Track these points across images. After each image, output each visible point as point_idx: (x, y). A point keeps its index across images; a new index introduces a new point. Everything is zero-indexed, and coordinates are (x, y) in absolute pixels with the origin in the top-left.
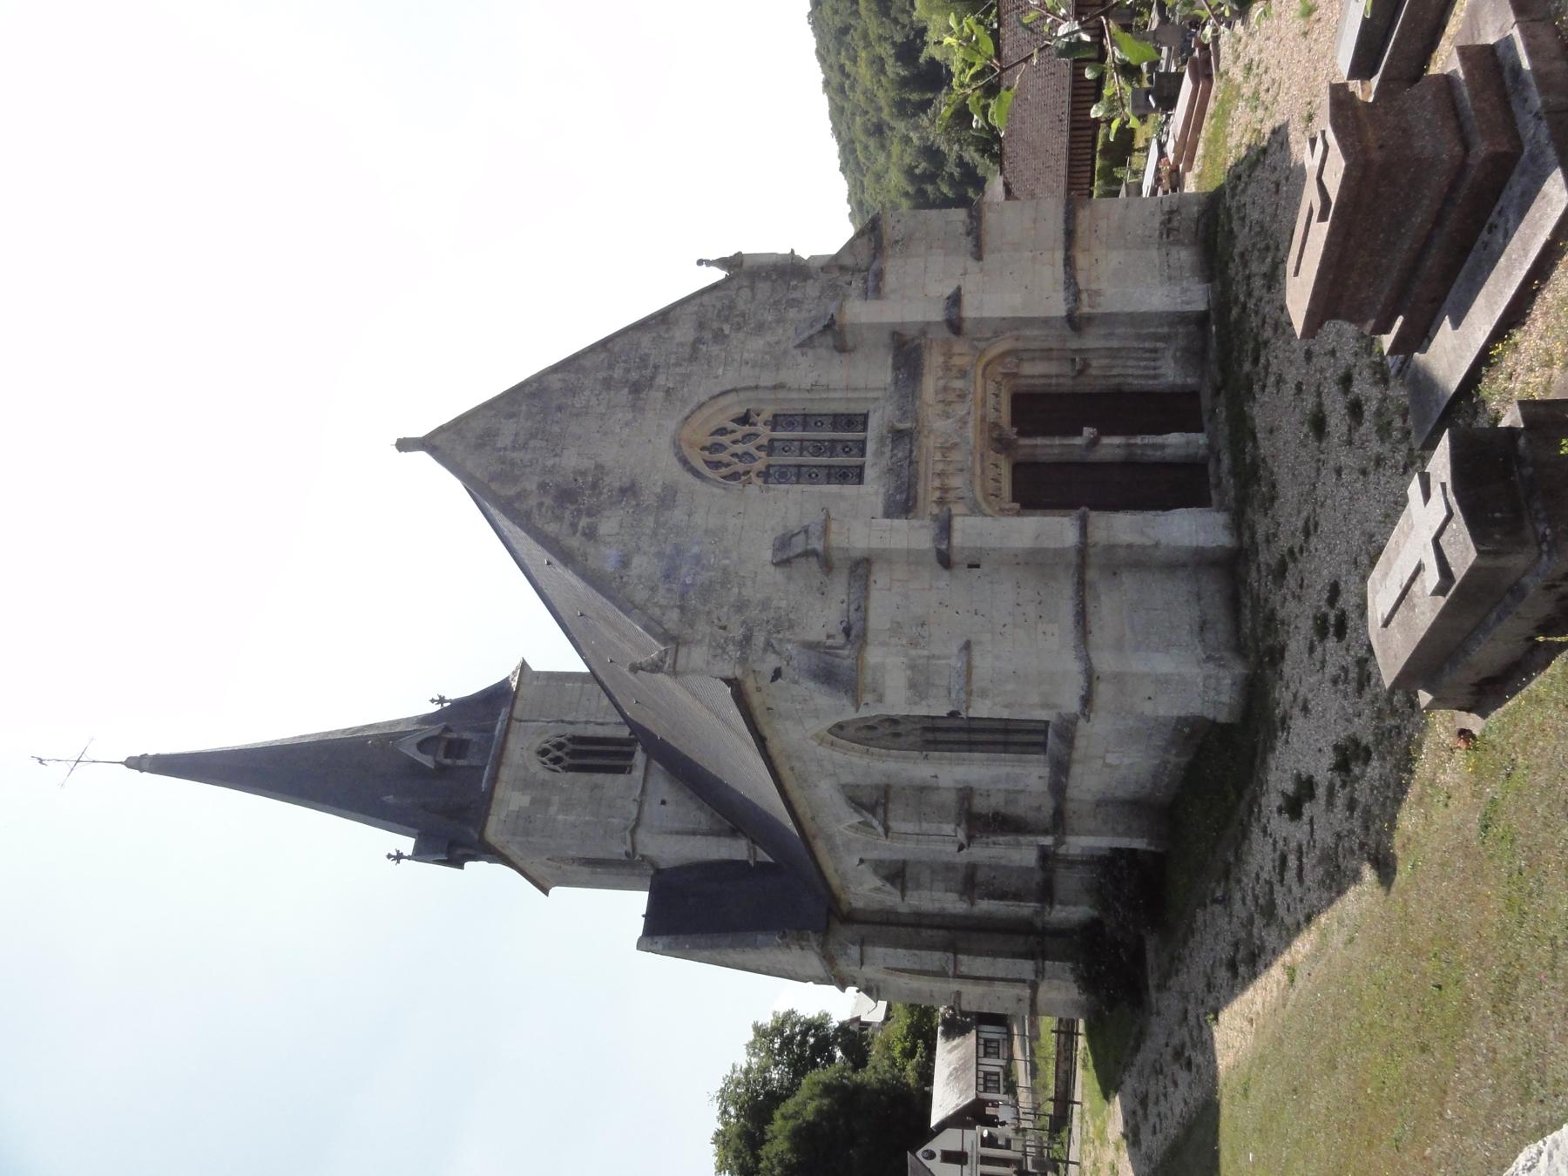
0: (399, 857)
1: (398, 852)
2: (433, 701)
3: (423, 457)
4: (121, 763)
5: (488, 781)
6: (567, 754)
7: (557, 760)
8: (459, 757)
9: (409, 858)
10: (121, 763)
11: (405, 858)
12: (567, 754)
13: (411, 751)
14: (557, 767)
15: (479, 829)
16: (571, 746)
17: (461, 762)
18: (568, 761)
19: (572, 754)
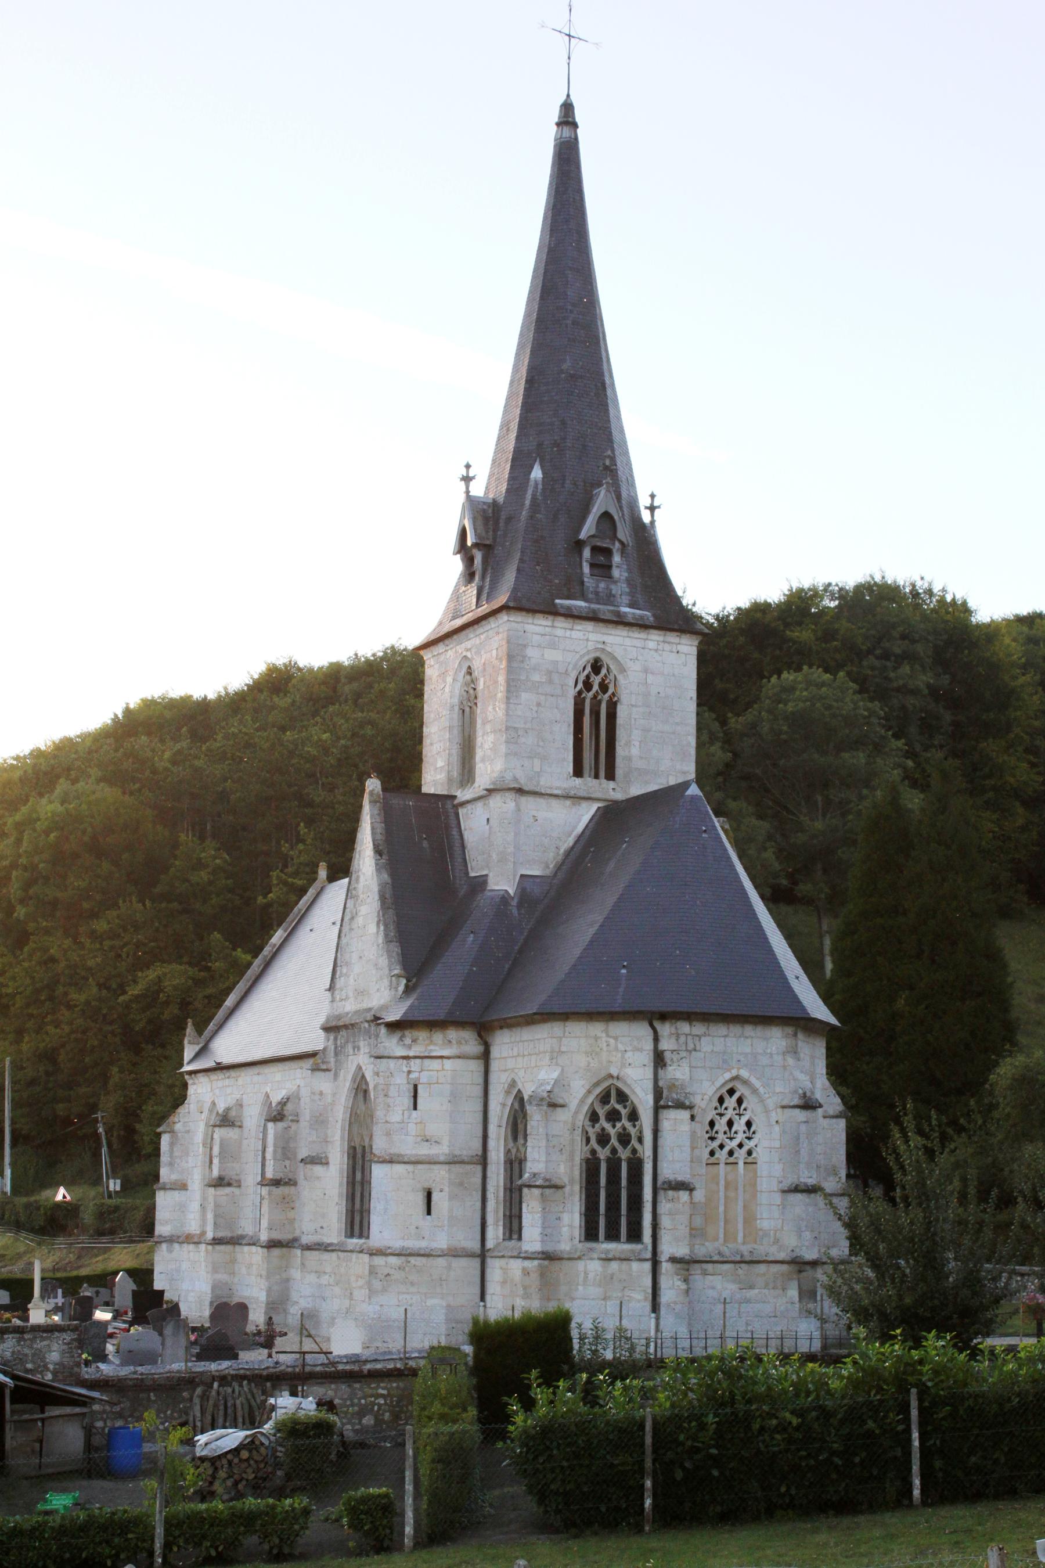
0: (467, 479)
1: (473, 478)
2: (653, 496)
3: (565, 97)
4: (568, 96)
5: (569, 608)
6: (595, 697)
7: (588, 685)
8: (592, 566)
9: (467, 492)
10: (568, 96)
11: (467, 487)
12: (614, 1151)
13: (602, 501)
14: (580, 685)
15: (511, 604)
16: (624, 1154)
17: (586, 569)
18: (603, 1154)
19: (614, 1165)
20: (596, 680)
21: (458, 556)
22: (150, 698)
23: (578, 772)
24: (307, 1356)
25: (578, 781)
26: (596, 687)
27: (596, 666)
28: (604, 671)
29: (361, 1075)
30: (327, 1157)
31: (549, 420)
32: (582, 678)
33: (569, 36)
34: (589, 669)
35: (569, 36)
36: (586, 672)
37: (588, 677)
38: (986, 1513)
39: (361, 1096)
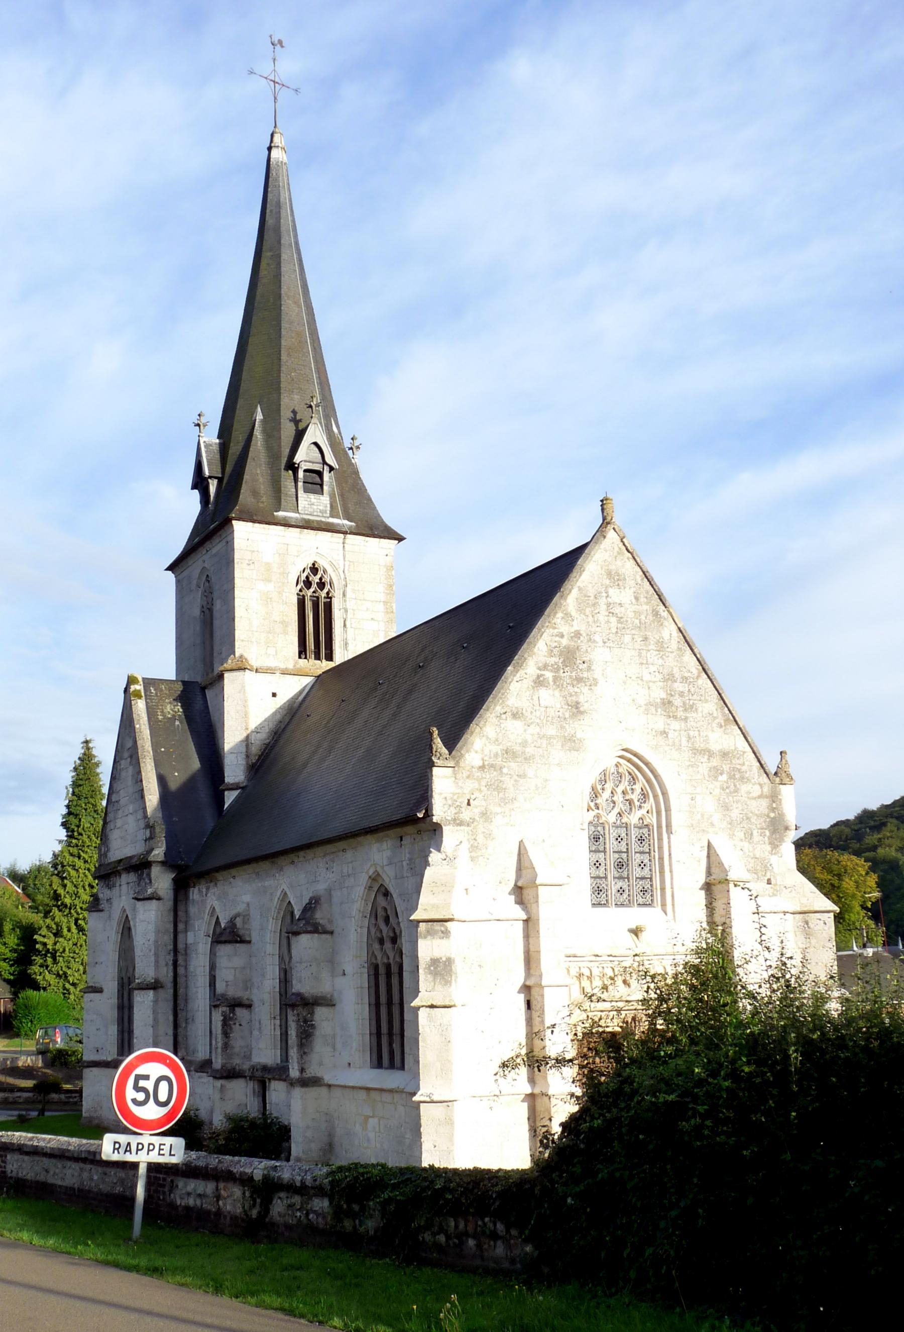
5: (285, 518)
7: (308, 583)
14: (301, 584)
20: (315, 579)
21: (196, 492)
22: (513, 897)
23: (302, 652)
24: (603, 854)
25: (303, 662)
26: (314, 587)
27: (314, 570)
28: (327, 587)
29: (125, 916)
30: (101, 988)
31: (623, 1114)
32: (303, 577)
33: (274, 82)
34: (308, 571)
35: (274, 82)
36: (305, 574)
37: (307, 577)
38: (301, 355)
39: (126, 932)
